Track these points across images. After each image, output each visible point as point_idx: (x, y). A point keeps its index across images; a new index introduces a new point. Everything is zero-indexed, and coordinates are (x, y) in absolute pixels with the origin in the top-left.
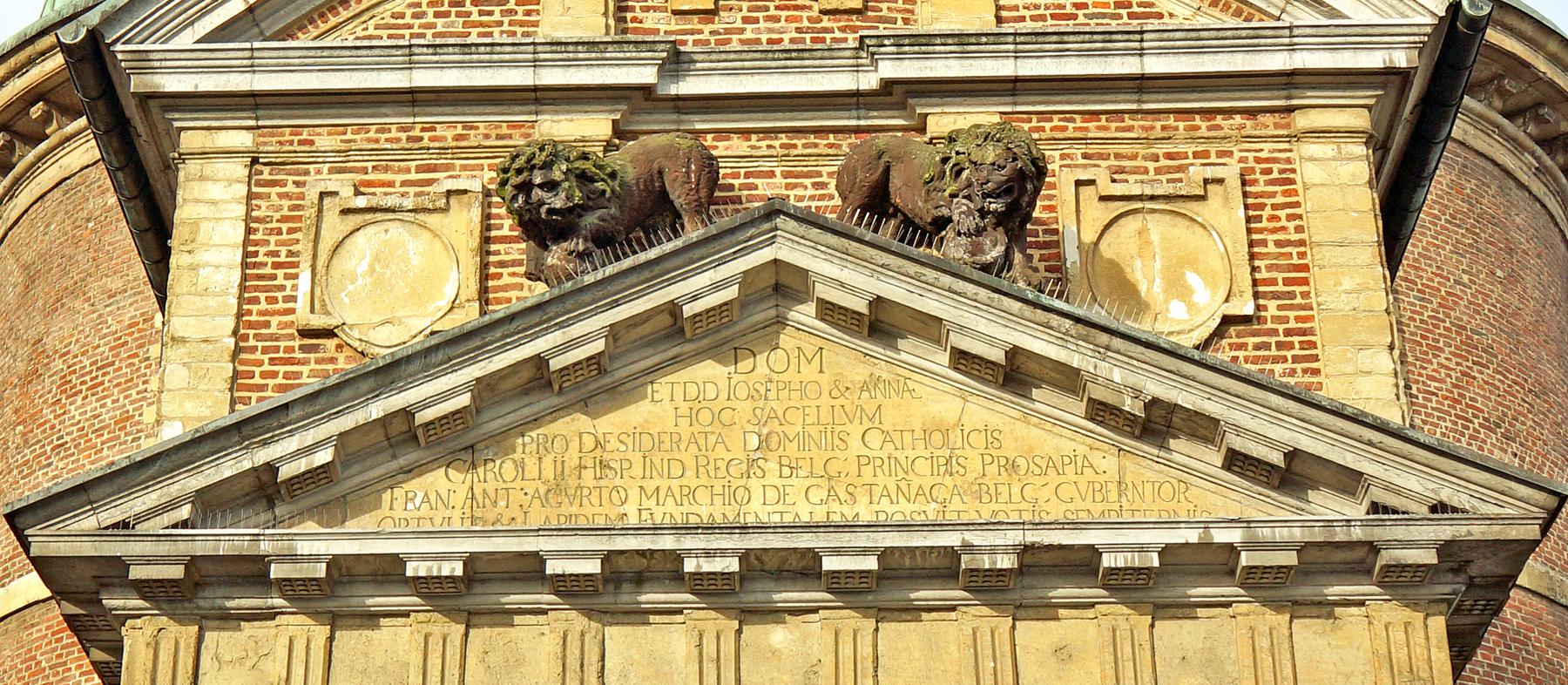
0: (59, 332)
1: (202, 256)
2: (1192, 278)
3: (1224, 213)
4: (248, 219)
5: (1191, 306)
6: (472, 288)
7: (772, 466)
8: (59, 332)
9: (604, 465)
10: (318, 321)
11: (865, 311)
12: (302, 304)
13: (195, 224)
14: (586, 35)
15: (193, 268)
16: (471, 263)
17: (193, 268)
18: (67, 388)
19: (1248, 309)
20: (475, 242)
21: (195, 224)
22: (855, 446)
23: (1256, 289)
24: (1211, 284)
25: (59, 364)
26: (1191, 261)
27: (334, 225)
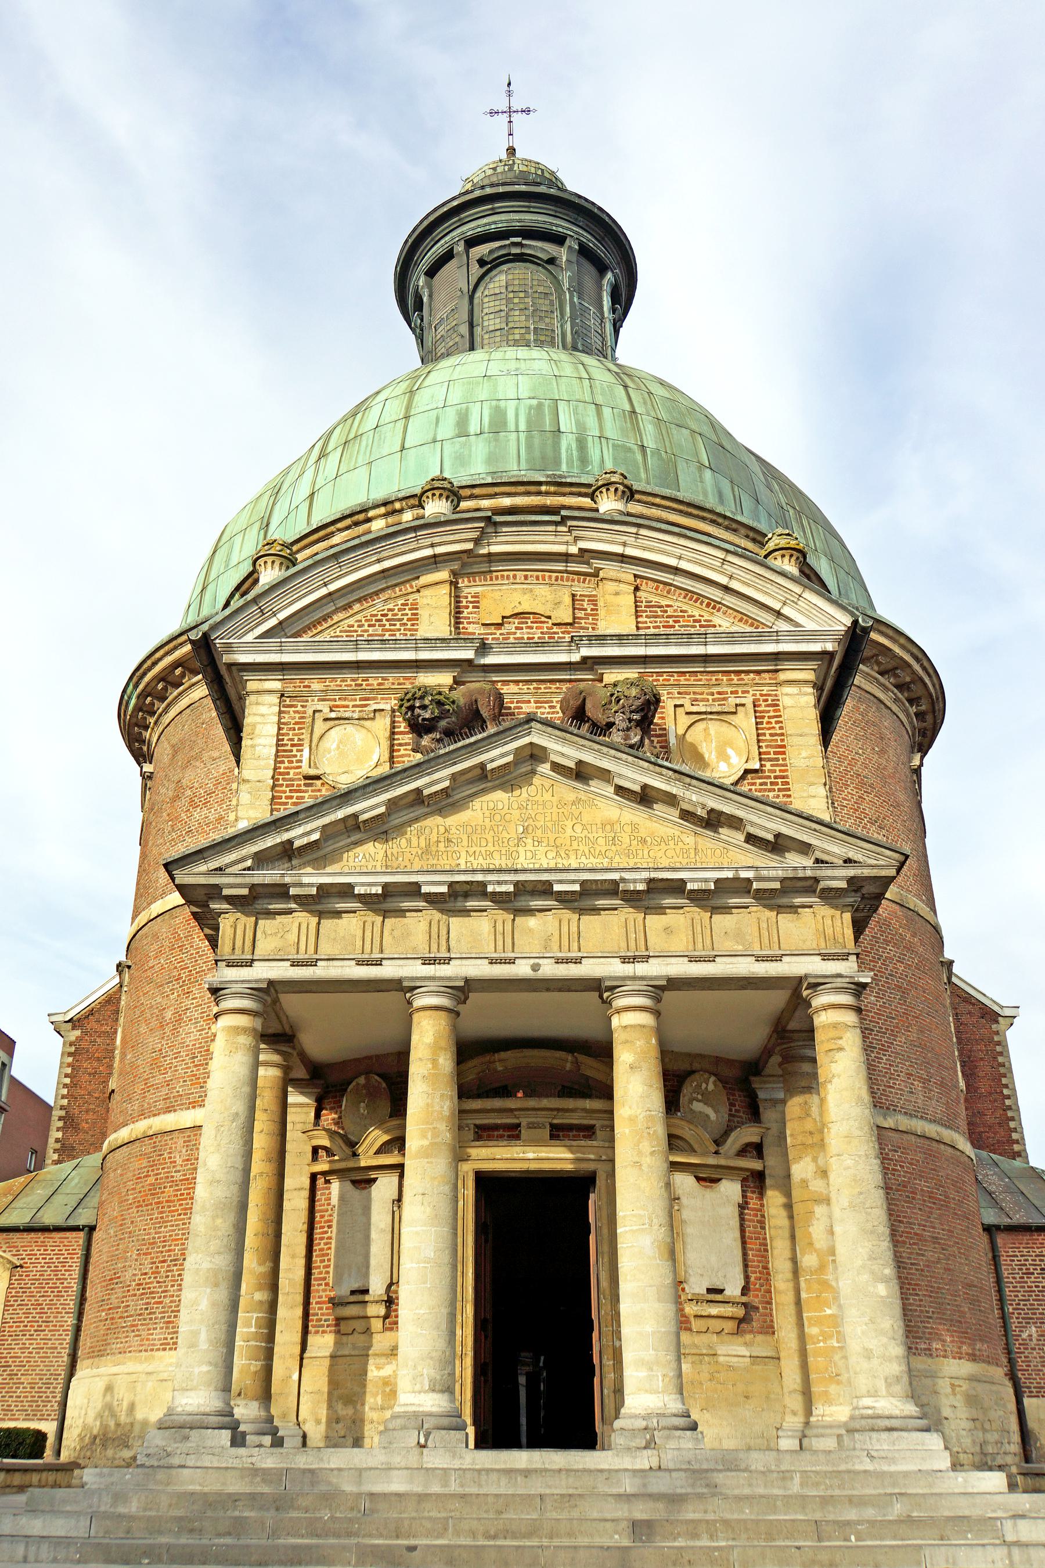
0: (189, 777)
2: (730, 751)
4: (279, 723)
5: (729, 764)
6: (387, 756)
8: (189, 777)
9: (449, 841)
10: (312, 772)
12: (305, 764)
13: (254, 726)
15: (253, 746)
16: (385, 744)
17: (253, 746)
21: (254, 726)
22: (569, 832)
24: (739, 754)
25: (189, 793)
27: (320, 726)
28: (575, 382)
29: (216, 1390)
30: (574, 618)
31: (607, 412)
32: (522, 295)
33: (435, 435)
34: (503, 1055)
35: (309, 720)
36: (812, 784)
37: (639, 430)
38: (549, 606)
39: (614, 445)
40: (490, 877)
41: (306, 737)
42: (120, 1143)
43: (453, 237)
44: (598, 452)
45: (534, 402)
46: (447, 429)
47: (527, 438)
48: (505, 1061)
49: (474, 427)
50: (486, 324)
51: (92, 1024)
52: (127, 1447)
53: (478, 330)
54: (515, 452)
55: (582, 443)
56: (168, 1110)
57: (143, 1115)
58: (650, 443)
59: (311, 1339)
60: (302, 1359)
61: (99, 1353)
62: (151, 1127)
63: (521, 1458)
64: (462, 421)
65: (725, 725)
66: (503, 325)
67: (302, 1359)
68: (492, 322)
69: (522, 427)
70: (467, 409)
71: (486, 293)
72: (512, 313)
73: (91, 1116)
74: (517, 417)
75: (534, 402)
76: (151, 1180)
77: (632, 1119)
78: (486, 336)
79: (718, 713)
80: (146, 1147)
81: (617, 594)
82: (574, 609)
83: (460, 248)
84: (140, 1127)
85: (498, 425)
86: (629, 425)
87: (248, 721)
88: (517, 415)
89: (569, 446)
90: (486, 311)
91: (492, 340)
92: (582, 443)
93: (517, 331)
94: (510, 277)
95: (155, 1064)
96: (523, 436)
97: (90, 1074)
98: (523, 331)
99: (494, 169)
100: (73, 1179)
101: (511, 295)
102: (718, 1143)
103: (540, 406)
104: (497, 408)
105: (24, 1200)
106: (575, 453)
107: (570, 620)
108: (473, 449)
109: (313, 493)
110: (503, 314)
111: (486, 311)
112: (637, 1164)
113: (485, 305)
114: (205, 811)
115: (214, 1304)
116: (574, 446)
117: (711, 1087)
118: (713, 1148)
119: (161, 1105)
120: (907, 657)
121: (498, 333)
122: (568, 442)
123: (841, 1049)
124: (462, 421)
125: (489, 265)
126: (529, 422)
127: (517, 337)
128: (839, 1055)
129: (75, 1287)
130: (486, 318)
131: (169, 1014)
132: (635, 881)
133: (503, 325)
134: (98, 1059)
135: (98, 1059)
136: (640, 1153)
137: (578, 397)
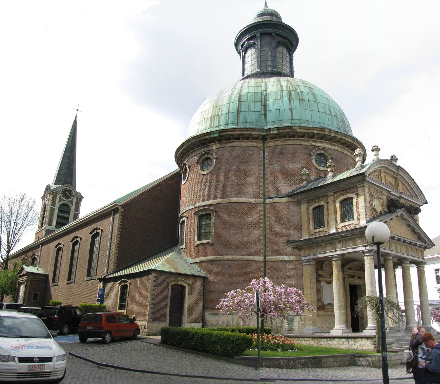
0: (242, 167)
8: (242, 167)
56: (249, 255)
58: (272, 132)
83: (258, 35)
114: (251, 179)
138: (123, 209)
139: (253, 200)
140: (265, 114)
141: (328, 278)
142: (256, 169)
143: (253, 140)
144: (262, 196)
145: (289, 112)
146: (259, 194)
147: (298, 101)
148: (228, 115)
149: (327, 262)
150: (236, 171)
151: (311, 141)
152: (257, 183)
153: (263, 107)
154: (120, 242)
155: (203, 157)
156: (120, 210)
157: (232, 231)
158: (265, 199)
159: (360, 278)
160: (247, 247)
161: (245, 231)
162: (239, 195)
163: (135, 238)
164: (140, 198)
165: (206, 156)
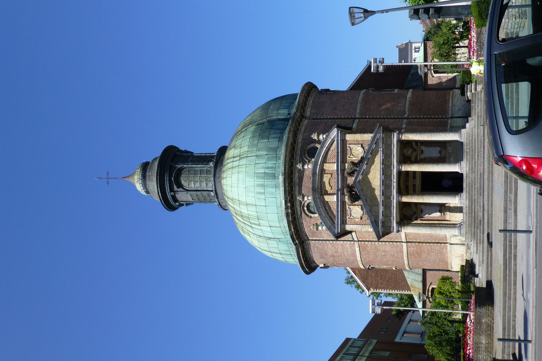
0: (330, 254)
1: (354, 228)
2: (357, 149)
3: (352, 146)
4: (350, 224)
5: (360, 149)
6: (357, 206)
7: (373, 183)
8: (330, 254)
9: (373, 196)
10: (360, 218)
11: (320, 90)
12: (358, 220)
13: (351, 229)
14: (458, 271)
15: (355, 229)
16: (355, 206)
17: (355, 229)
18: (336, 252)
19: (360, 145)
20: (353, 206)
21: (351, 229)
22: (372, 176)
23: (354, 130)
24: (358, 148)
25: (334, 253)
26: (356, 149)
27: (352, 217)
28: (247, 168)
29: (456, 198)
30: (330, 174)
31: (257, 162)
32: (189, 177)
33: (263, 199)
34: (401, 186)
35: (350, 219)
36: (364, 136)
37: (262, 155)
38: (327, 178)
39: (267, 161)
40: (381, 189)
41: (353, 220)
42: (408, 263)
43: (169, 195)
44: (269, 164)
45: (255, 178)
46: (262, 197)
47: (266, 179)
48: (402, 187)
49: (263, 191)
50: (197, 187)
51: (369, 286)
52: (463, 255)
53: (199, 189)
54: (270, 182)
55: (267, 168)
56: (403, 252)
57: (403, 258)
59: (447, 219)
60: (450, 221)
61: (447, 263)
62: (406, 256)
63: (464, 186)
64: (261, 193)
65: (353, 150)
66: (199, 182)
67: (450, 221)
68: (197, 185)
69: (263, 180)
70: (257, 192)
71: (187, 187)
72: (195, 180)
73: (392, 284)
74: (261, 181)
75: (255, 178)
76: (416, 255)
77: (418, 169)
78: (201, 187)
79: (350, 151)
80: (409, 257)
81: (326, 166)
82: (328, 174)
83: (172, 194)
84: (405, 258)
85: (263, 186)
86: (260, 157)
87: (350, 230)
88: (259, 181)
89: (268, 171)
90: (193, 187)
91: (203, 186)
92: (267, 168)
93: (201, 179)
94: (183, 180)
95: (392, 256)
96: (265, 180)
97: (381, 285)
98: (201, 177)
99: (140, 184)
100: (411, 278)
101: (189, 180)
102: (415, 150)
103: (256, 176)
104: (257, 186)
105: (416, 286)
106: (270, 170)
107: (331, 175)
108: (268, 191)
109: (270, 226)
110: (195, 182)
111: (193, 187)
112: (425, 168)
113: (191, 187)
114: (339, 249)
115: (444, 229)
116: (268, 170)
117: (405, 150)
118: (417, 151)
119: (401, 254)
120: (499, 224)
121: (201, 184)
122: (267, 171)
123: (408, 137)
124: (261, 193)
125: (180, 185)
126: (262, 179)
127: (202, 179)
128: (409, 137)
129: (434, 272)
130: (195, 187)
131: (383, 254)
132: (382, 167)
133: (193, 182)
134: (378, 283)
135: (378, 283)
136: (423, 168)
137: (253, 168)
138: (371, 288)
139: (357, 249)
140: (279, 239)
141: (418, 214)
142: (330, 245)
143: (305, 248)
144: (352, 242)
145: (272, 228)
146: (350, 244)
147: (259, 220)
148: (254, 205)
149: (404, 212)
150: (334, 257)
151: (297, 217)
152: (342, 245)
153: (271, 239)
154: (399, 290)
155: (306, 211)
156: (373, 291)
157: (385, 260)
158: (354, 241)
159: (414, 177)
160: (396, 253)
161: (383, 254)
162: (354, 255)
163: (392, 277)
164: (359, 275)
165: (305, 209)
